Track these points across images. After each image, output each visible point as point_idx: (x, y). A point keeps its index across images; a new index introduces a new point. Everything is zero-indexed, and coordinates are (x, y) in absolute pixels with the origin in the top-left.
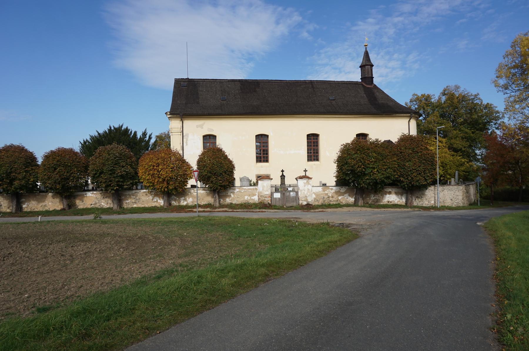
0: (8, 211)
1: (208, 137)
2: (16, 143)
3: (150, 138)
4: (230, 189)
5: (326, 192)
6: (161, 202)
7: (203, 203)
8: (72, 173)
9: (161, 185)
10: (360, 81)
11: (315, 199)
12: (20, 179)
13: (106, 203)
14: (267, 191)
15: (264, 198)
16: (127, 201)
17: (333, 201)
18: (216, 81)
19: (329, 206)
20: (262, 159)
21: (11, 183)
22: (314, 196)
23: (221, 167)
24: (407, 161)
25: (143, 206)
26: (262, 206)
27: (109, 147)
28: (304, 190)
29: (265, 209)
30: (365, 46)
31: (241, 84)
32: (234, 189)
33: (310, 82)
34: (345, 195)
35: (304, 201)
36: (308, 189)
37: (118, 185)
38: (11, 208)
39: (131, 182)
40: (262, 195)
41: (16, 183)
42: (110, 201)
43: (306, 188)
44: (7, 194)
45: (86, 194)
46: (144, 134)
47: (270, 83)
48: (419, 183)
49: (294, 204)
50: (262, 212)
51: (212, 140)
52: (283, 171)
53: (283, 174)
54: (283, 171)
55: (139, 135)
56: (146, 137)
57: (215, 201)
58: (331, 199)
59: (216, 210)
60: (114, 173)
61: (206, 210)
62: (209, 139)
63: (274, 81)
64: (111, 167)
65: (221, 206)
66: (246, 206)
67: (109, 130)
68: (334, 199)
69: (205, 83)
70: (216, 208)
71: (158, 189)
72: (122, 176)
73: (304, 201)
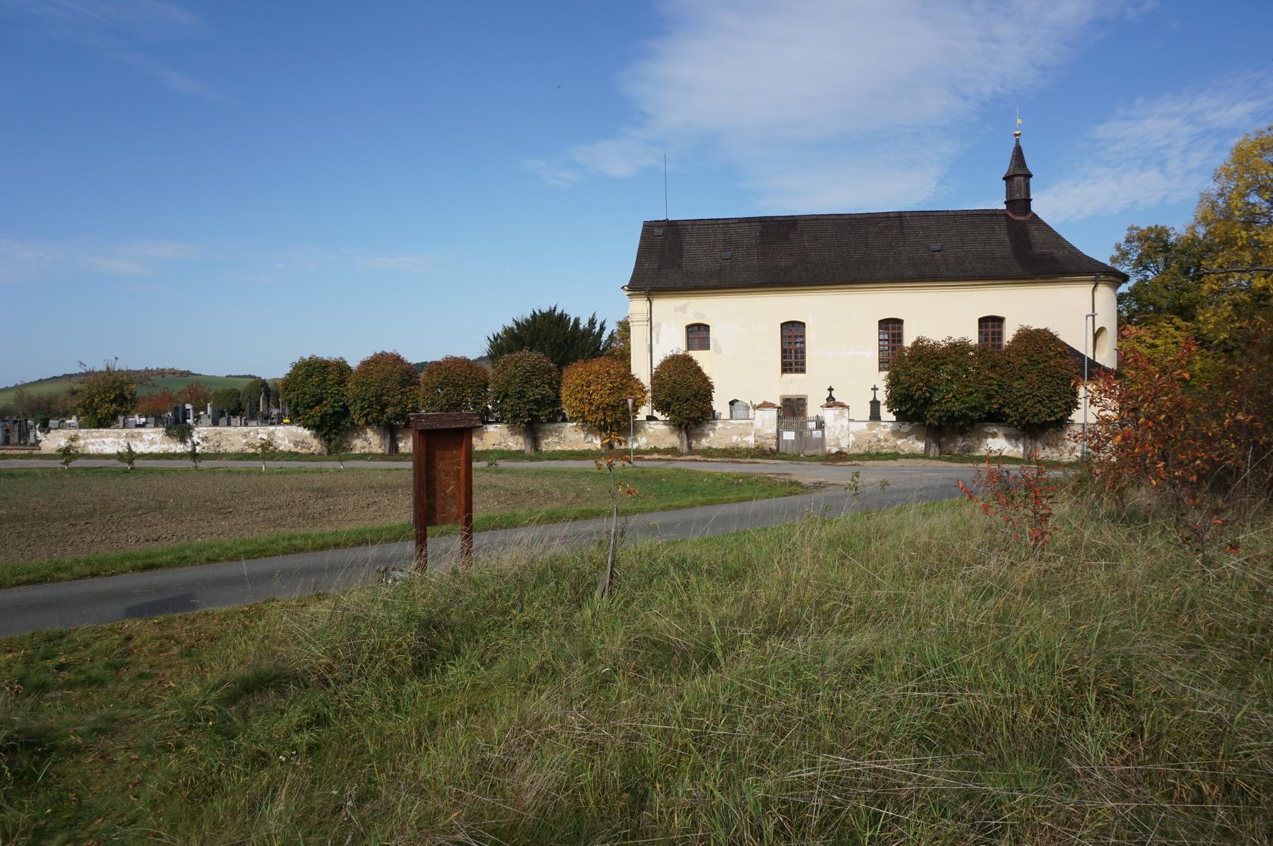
0: (380, 451)
1: (696, 328)
2: (389, 350)
3: (602, 328)
4: (708, 423)
5: (874, 431)
6: (597, 443)
7: (663, 446)
8: (464, 397)
9: (595, 416)
10: (1004, 207)
11: (854, 443)
12: (394, 405)
13: (516, 443)
14: (770, 428)
15: (763, 440)
16: (547, 441)
17: (887, 448)
18: (717, 222)
19: (878, 456)
20: (794, 367)
21: (382, 411)
22: (852, 438)
23: (687, 388)
24: (1018, 379)
25: (570, 449)
26: (760, 453)
27: (517, 355)
28: (835, 428)
29: (761, 458)
30: (1016, 135)
31: (762, 227)
32: (715, 424)
33: (897, 215)
34: (909, 437)
35: (835, 446)
36: (842, 427)
37: (530, 416)
38: (383, 448)
39: (551, 410)
40: (761, 434)
41: (389, 410)
42: (521, 440)
43: (838, 424)
44: (378, 426)
45: (486, 428)
46: (592, 322)
47: (819, 221)
48: (1040, 419)
49: (820, 451)
50: (755, 463)
51: (703, 334)
52: (831, 389)
53: (831, 394)
54: (831, 389)
55: (584, 323)
56: (594, 328)
57: (682, 442)
58: (882, 444)
59: (681, 458)
60: (524, 396)
61: (664, 457)
62: (698, 334)
63: (825, 217)
64: (519, 387)
65: (691, 451)
66: (732, 453)
67: (532, 317)
68: (888, 444)
69: (696, 227)
70: (682, 454)
71: (591, 422)
72: (536, 401)
73: (835, 446)
